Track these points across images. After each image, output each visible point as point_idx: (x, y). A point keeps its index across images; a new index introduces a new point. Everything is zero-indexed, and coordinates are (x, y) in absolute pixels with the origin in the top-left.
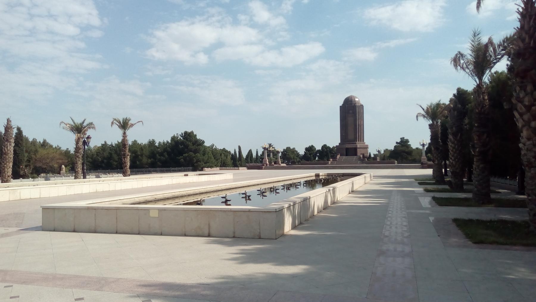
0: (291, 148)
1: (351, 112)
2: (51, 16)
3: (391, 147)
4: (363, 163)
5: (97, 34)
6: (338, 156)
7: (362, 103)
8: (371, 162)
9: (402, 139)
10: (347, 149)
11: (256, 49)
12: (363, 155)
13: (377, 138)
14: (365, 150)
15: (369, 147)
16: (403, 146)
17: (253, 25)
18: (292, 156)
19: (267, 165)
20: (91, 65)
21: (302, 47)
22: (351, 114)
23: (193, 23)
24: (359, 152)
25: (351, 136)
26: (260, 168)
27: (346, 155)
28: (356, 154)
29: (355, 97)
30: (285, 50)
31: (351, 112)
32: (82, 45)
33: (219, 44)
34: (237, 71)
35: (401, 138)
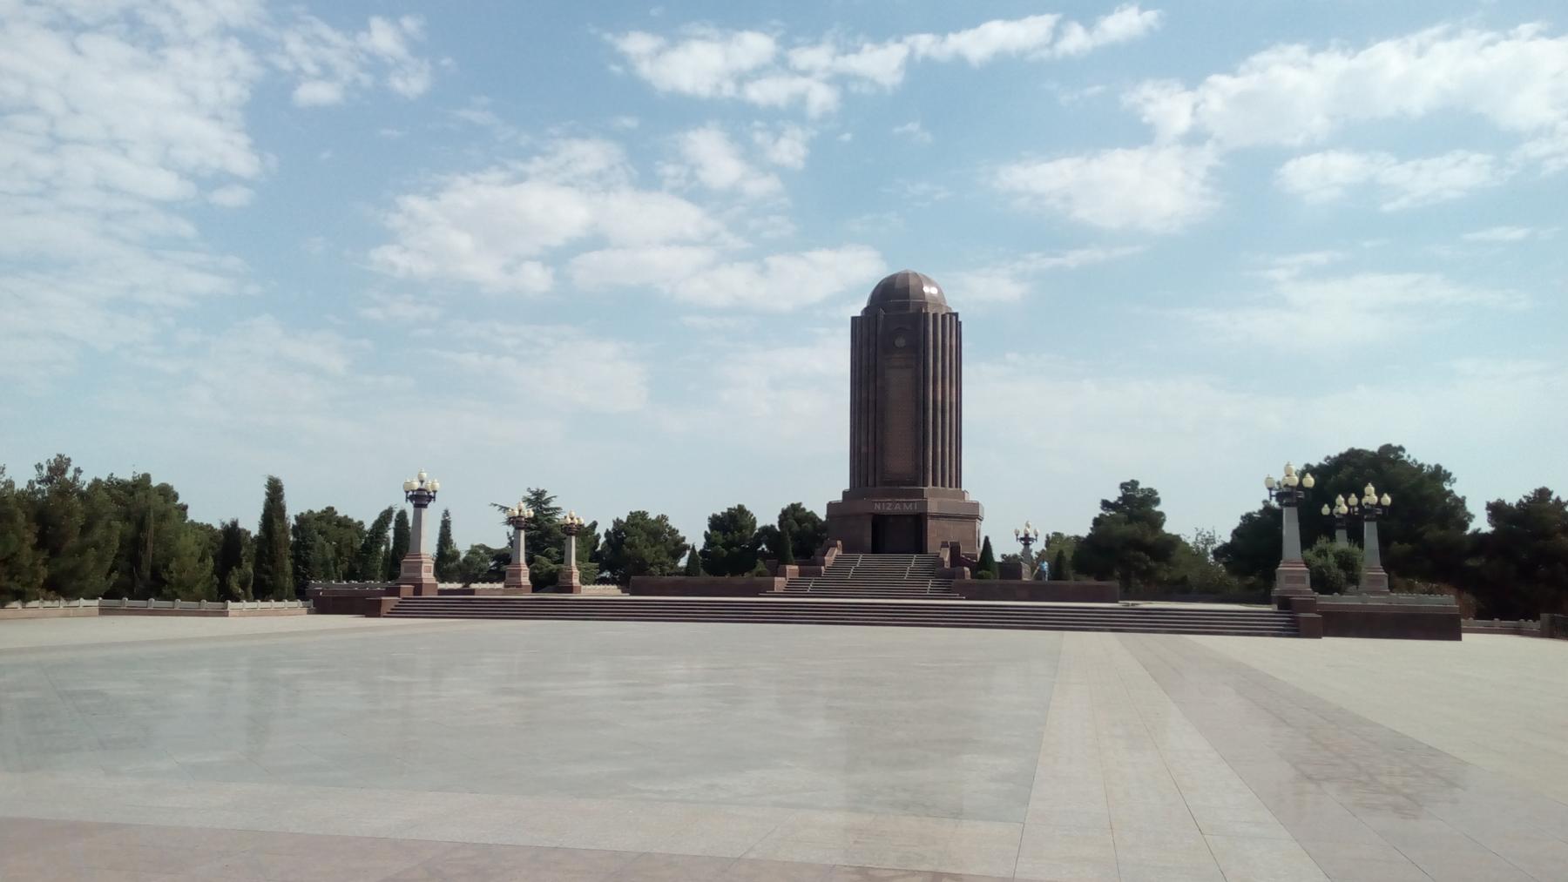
0: (652, 516)
1: (900, 342)
2: (118, 146)
3: (1080, 526)
4: (948, 591)
5: (232, 198)
6: (833, 555)
7: (954, 303)
8: (989, 587)
9: (1129, 487)
10: (879, 522)
11: (697, 256)
12: (955, 550)
13: (1023, 475)
14: (965, 526)
15: (987, 512)
16: (1132, 518)
17: (697, 194)
18: (648, 553)
19: (418, 588)
20: (204, 284)
21: (823, 256)
22: (902, 358)
23: (521, 178)
24: (936, 534)
25: (898, 462)
26: (369, 607)
27: (876, 548)
28: (919, 546)
29: (921, 280)
30: (775, 261)
31: (900, 342)
32: (187, 229)
33: (596, 241)
34: (633, 314)
35: (1123, 486)
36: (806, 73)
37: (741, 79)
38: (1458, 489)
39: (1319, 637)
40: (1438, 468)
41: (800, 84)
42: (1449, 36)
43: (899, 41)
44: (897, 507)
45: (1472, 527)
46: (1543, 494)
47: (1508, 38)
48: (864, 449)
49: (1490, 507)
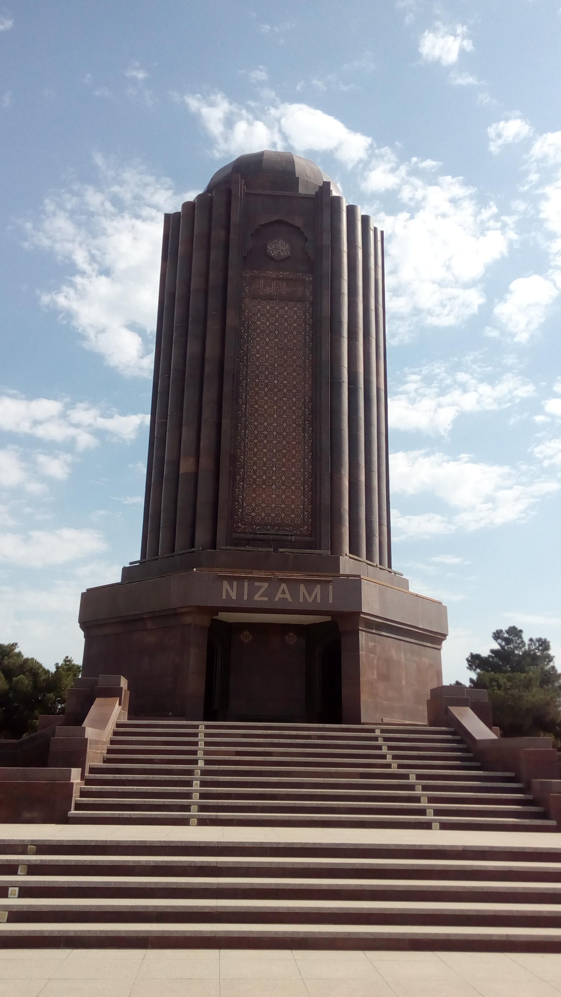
6: (104, 724)
10: (222, 639)
25: (271, 495)
27: (214, 708)
30: (35, 534)
35: (497, 635)
36: (77, 426)
37: (36, 423)
41: (72, 431)
42: (428, 455)
43: (231, 103)
44: (283, 594)
47: (455, 460)
48: (186, 466)
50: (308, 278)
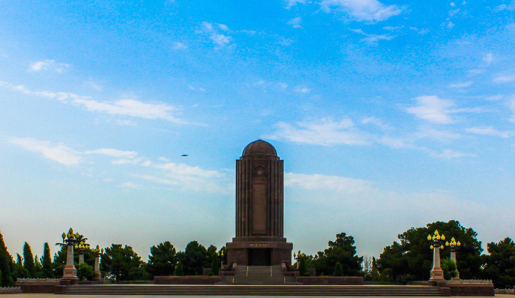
1: (260, 172)
10: (251, 252)
25: (260, 225)
27: (250, 264)
35: (338, 236)
38: (478, 238)
39: (449, 296)
40: (470, 230)
44: (260, 245)
45: (482, 254)
46: (508, 240)
49: (489, 245)
50: (266, 179)
